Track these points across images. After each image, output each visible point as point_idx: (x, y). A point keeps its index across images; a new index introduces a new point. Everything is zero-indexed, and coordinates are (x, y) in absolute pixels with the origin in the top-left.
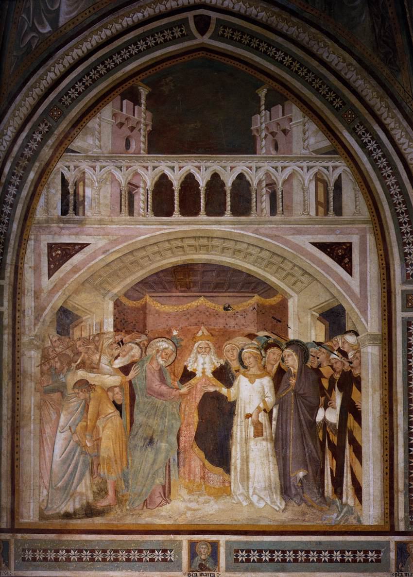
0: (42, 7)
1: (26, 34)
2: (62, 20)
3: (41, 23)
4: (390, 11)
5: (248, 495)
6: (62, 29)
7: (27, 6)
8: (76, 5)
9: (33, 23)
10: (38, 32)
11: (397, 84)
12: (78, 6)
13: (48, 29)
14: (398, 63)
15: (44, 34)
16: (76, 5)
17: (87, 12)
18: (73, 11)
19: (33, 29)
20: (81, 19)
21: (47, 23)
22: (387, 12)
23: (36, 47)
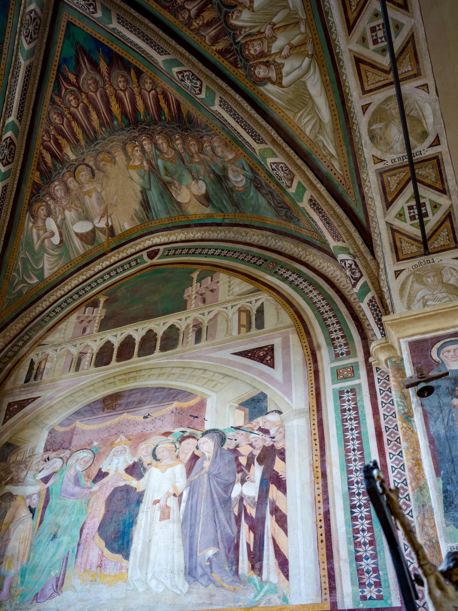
0: (29, 268)
1: (17, 284)
2: (47, 274)
3: (30, 277)
4: (272, 186)
5: (79, 86)
6: (48, 280)
7: (17, 267)
8: (56, 263)
9: (23, 278)
10: (28, 283)
11: (303, 230)
12: (58, 264)
13: (35, 280)
14: (295, 215)
15: (32, 284)
16: (56, 263)
17: (66, 267)
18: (55, 267)
19: (23, 281)
20: (61, 272)
21: (33, 275)
22: (271, 188)
23: (27, 293)
